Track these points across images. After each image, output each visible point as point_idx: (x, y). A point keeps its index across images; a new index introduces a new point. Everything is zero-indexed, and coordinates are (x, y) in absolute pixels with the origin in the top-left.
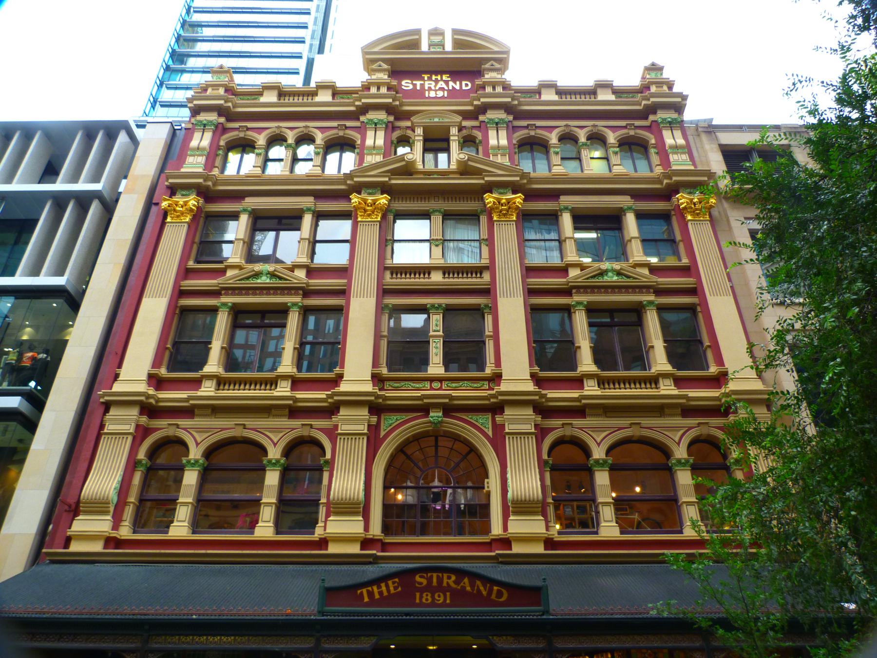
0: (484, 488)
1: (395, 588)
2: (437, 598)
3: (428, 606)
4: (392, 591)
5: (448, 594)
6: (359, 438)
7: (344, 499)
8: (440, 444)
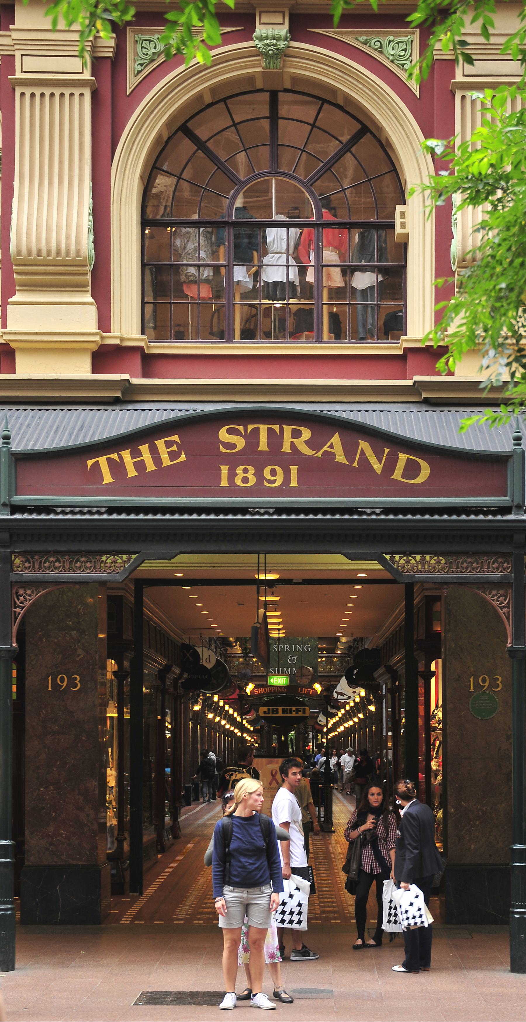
0: (392, 226)
1: (173, 456)
2: (270, 477)
3: (279, 491)
4: (166, 461)
5: (294, 469)
6: (72, 95)
7: (44, 252)
8: (283, 110)
